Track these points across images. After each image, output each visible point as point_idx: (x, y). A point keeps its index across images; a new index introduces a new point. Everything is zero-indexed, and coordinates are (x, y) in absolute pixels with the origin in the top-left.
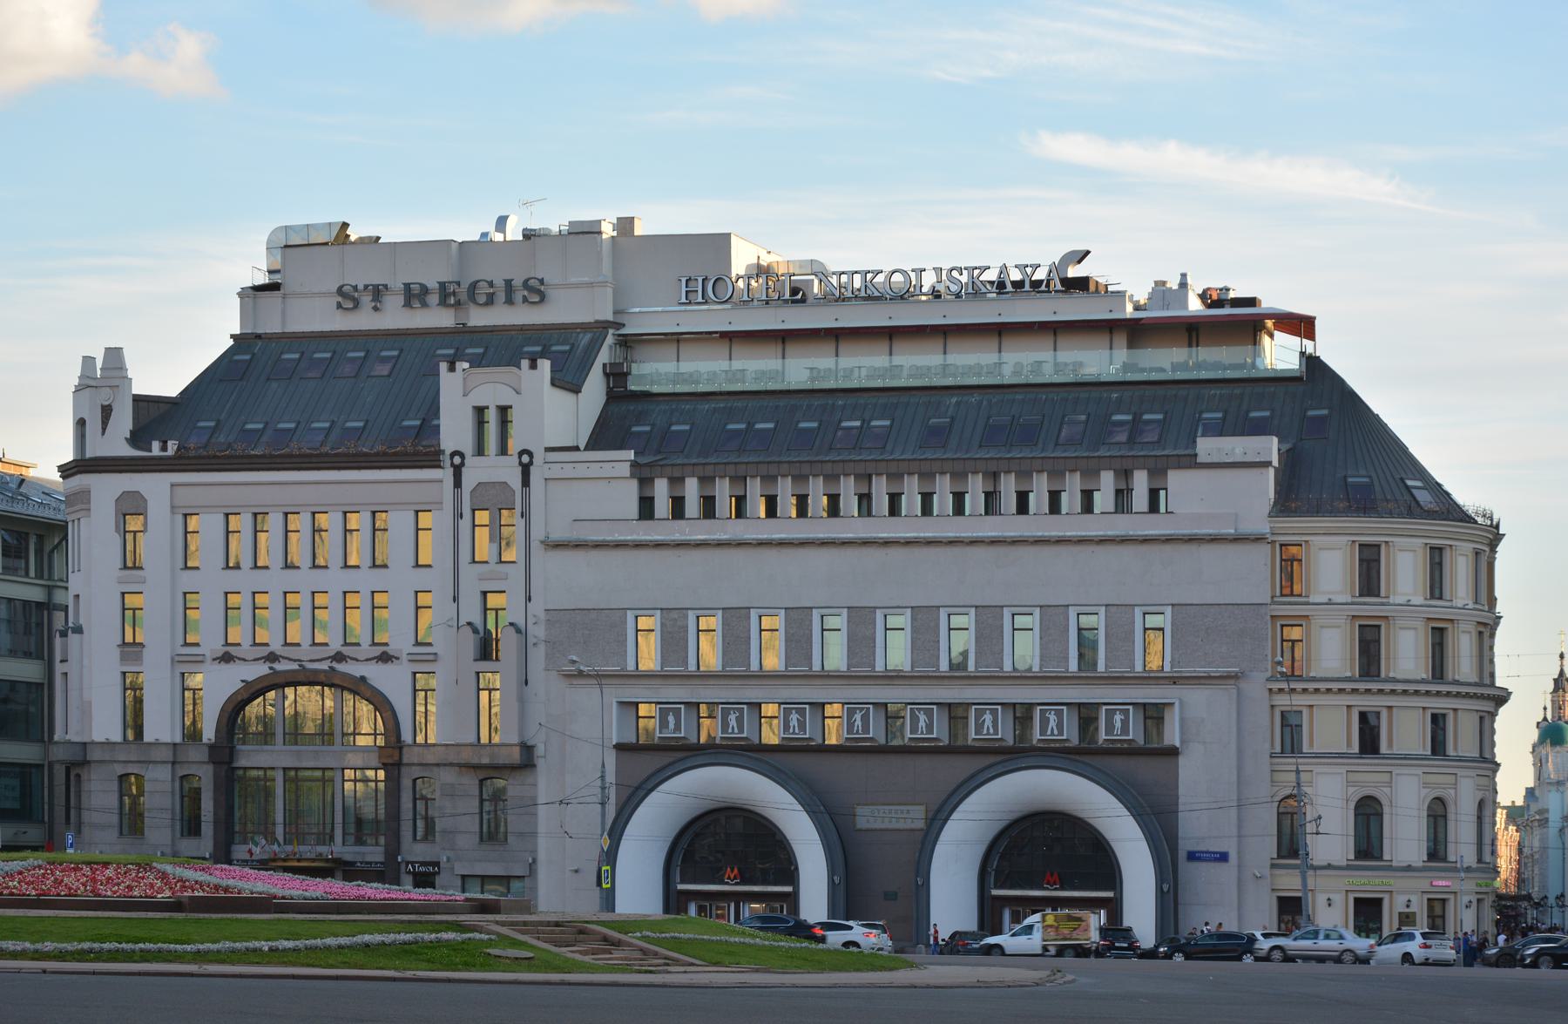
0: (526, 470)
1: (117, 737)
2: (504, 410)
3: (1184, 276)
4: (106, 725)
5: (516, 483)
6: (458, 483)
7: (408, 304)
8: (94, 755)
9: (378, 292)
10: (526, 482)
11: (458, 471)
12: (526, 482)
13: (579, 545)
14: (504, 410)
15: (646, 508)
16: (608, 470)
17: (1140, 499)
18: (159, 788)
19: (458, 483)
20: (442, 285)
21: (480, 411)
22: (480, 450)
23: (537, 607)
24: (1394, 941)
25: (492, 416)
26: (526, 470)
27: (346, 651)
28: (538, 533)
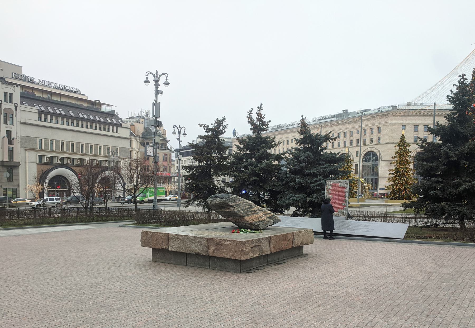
0: (16, 107)
2: (11, 94)
5: (14, 109)
14: (11, 94)
16: (33, 111)
22: (6, 101)
23: (19, 135)
26: (16, 107)
28: (19, 120)
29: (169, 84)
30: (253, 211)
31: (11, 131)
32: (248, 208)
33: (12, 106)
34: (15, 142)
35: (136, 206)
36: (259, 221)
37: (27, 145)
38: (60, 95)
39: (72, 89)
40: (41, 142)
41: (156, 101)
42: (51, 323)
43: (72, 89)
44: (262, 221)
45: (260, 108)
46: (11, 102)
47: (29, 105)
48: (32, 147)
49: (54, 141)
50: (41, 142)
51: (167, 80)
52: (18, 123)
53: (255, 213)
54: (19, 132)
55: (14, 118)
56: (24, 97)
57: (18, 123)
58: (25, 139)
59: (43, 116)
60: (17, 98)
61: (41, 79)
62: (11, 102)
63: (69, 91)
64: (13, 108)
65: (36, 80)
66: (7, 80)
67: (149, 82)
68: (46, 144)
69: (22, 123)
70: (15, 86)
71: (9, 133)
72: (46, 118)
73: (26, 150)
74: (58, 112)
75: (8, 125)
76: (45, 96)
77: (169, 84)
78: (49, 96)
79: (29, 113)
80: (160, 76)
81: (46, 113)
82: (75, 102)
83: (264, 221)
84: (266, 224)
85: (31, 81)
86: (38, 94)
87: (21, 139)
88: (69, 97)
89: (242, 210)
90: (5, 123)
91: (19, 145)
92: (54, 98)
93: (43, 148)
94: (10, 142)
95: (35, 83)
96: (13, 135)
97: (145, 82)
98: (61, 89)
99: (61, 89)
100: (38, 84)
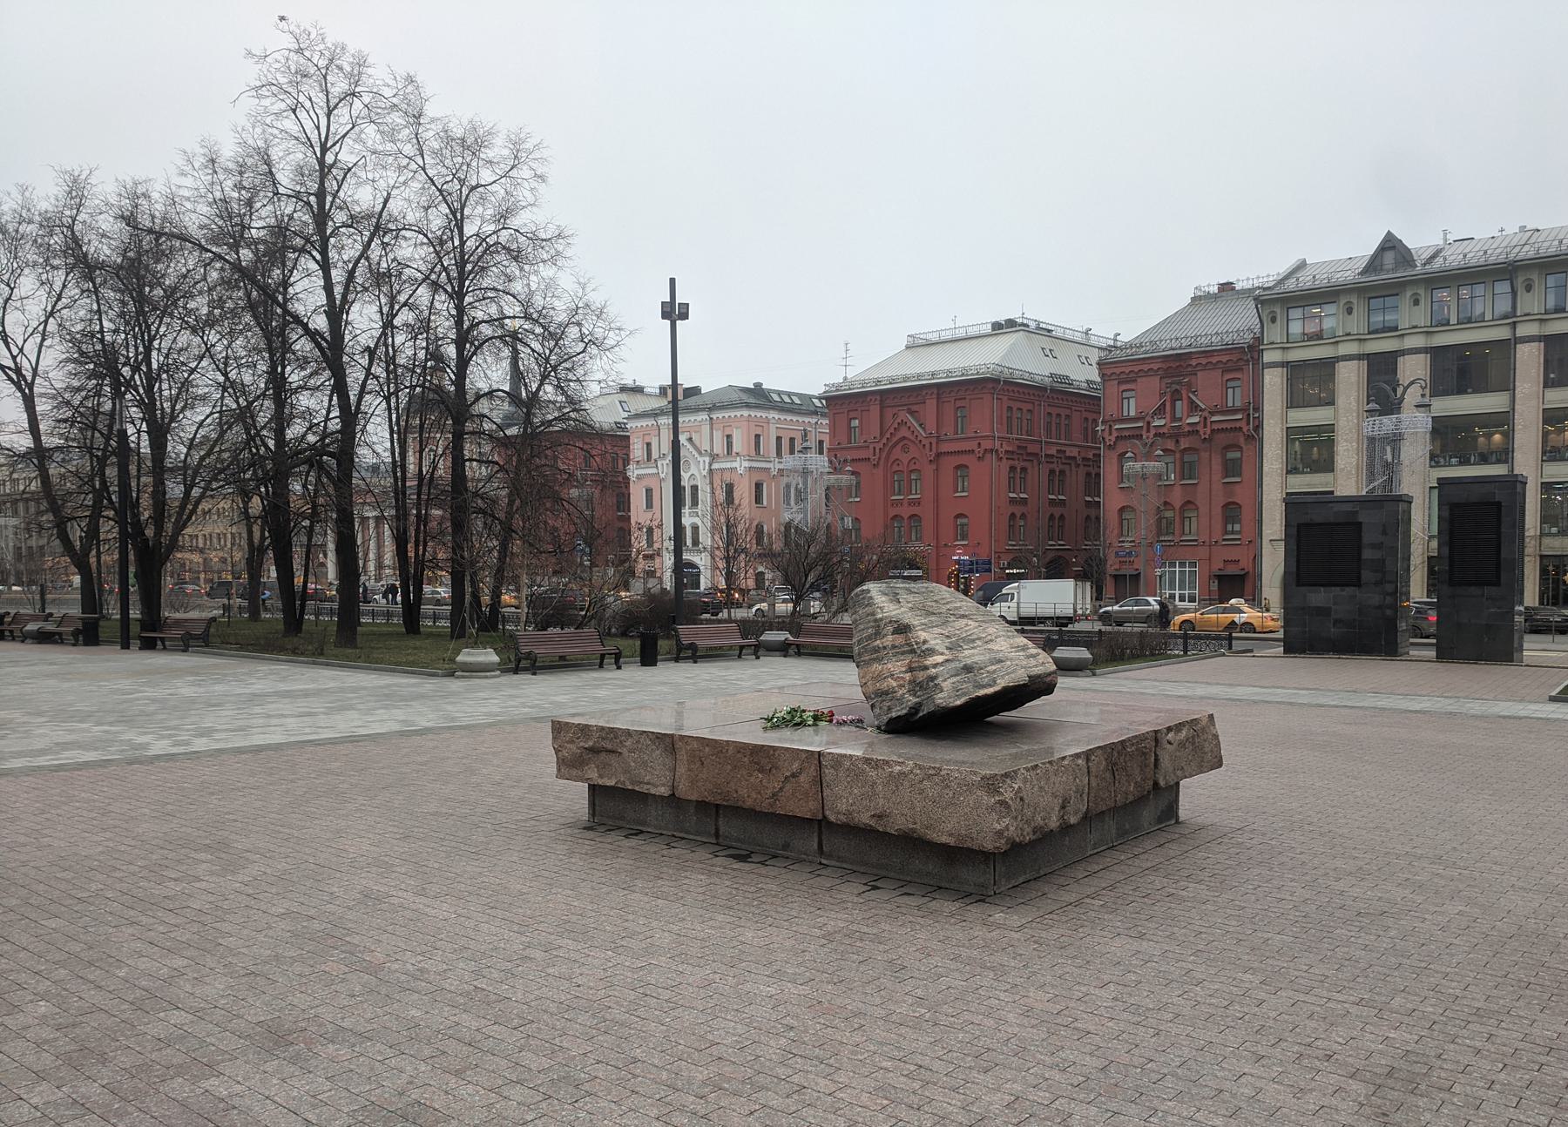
83: (886, 693)
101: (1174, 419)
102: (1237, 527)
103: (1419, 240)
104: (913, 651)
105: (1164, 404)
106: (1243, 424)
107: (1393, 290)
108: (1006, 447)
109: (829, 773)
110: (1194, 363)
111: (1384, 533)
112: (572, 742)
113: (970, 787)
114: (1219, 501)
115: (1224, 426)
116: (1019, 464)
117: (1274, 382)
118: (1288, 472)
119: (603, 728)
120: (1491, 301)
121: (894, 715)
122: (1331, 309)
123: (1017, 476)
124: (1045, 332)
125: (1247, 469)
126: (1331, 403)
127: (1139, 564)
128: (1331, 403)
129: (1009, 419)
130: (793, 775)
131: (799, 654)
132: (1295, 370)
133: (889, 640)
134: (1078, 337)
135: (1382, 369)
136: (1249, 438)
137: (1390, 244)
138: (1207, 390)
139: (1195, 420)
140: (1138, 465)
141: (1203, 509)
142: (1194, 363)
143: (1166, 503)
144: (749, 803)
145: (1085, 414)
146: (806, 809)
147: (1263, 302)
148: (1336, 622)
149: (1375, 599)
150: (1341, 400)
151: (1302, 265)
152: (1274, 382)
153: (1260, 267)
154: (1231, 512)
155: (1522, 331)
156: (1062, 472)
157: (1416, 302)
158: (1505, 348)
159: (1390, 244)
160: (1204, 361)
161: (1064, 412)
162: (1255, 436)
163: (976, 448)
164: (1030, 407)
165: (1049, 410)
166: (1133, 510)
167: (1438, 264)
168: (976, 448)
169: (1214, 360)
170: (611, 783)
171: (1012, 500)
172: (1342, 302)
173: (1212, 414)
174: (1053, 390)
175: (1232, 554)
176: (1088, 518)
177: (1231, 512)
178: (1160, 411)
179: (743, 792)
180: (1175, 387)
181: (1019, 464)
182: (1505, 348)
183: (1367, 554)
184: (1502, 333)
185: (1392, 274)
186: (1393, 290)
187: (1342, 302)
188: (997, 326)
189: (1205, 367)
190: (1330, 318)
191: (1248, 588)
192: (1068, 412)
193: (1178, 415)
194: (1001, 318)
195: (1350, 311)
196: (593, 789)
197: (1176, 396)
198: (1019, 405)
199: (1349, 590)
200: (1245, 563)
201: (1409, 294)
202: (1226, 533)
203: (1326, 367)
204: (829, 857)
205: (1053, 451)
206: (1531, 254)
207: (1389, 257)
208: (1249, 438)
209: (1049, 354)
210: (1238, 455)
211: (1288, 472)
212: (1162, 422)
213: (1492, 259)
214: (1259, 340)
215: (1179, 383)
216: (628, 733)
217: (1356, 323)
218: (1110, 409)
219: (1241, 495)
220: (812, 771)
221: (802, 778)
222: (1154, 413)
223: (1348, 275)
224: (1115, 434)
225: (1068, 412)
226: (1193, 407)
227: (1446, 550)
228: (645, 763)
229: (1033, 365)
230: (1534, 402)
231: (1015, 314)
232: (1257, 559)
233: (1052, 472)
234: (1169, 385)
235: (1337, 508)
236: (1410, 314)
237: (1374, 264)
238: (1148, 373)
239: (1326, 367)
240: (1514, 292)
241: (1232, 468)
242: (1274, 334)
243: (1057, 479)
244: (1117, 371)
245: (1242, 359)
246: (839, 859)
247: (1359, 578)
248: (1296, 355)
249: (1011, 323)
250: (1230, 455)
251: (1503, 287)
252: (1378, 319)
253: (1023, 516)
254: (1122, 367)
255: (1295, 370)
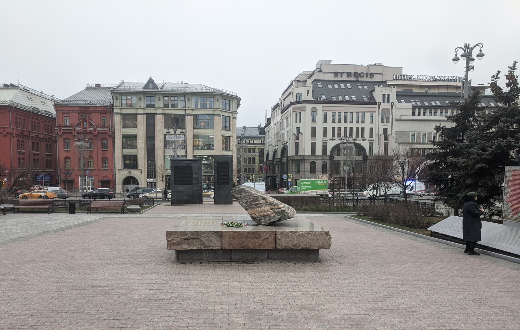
0: (392, 106)
1: (294, 154)
2: (389, 95)
3: (516, 63)
4: (308, 152)
5: (390, 108)
6: (379, 108)
7: (348, 76)
8: (305, 158)
9: (342, 73)
10: (392, 108)
11: (379, 106)
12: (392, 108)
13: (403, 120)
14: (389, 95)
15: (413, 114)
16: (408, 107)
17: (417, 113)
18: (319, 164)
19: (379, 108)
20: (354, 73)
21: (384, 95)
22: (384, 102)
23: (393, 131)
24: (431, 236)
25: (386, 96)
26: (392, 106)
27: (357, 138)
28: (394, 118)
29: (483, 55)
30: (256, 204)
31: (387, 128)
32: (252, 201)
33: (389, 106)
34: (390, 138)
35: (406, 199)
36: (261, 216)
37: (401, 140)
38: (438, 87)
39: (451, 78)
40: (413, 136)
41: (466, 78)
42: (176, 283)
43: (451, 78)
44: (264, 216)
45: (513, 68)
46: (388, 102)
47: (406, 103)
48: (405, 141)
49: (427, 133)
50: (413, 136)
51: (481, 51)
52: (394, 120)
53: (259, 207)
54: (394, 128)
55: (391, 116)
56: (400, 96)
57: (394, 120)
58: (400, 134)
59: (417, 110)
60: (393, 98)
61: (419, 75)
62: (388, 102)
63: (448, 81)
64: (390, 107)
65: (415, 77)
66: (388, 83)
67: (458, 59)
68: (419, 137)
69: (396, 120)
70: (392, 87)
71: (385, 130)
72: (436, 112)
73: (399, 144)
74: (434, 104)
75: (385, 123)
76: (423, 91)
77: (483, 55)
78: (427, 89)
79: (403, 110)
80: (472, 49)
81: (419, 108)
82: (444, 91)
83: (267, 216)
84: (269, 220)
85: (410, 79)
86: (415, 90)
87: (396, 134)
88: (447, 87)
89: (246, 203)
90: (383, 121)
91: (394, 140)
92: (432, 91)
93: (416, 141)
94: (386, 138)
95: (414, 80)
96: (389, 132)
97: (454, 60)
98: (439, 81)
99: (439, 81)
100: (417, 80)
101: (84, 128)
102: (107, 165)
103: (158, 81)
104: (270, 204)
105: (80, 122)
106: (108, 132)
107: (154, 95)
108: (15, 132)
109: (279, 236)
110: (90, 110)
111: (198, 170)
112: (178, 237)
113: (322, 235)
114: (100, 157)
115: (102, 132)
116: (21, 139)
117: (117, 119)
118: (123, 148)
119: (192, 232)
120: (180, 102)
121: (272, 221)
122: (134, 98)
123: (20, 144)
124: (25, 90)
125: (110, 146)
126: (136, 127)
127: (72, 177)
128: (136, 127)
129: (16, 122)
130: (267, 238)
131: (18, 212)
132: (124, 116)
133: (262, 202)
134: (40, 94)
135: (150, 119)
136: (110, 136)
137: (151, 81)
138: (96, 119)
139: (92, 129)
140: (80, 143)
141: (95, 159)
142: (90, 110)
143: (90, 156)
144: (251, 247)
145: (45, 123)
146: (270, 246)
147: (113, 93)
148: (186, 195)
149: (197, 189)
150: (139, 127)
151: (123, 83)
152: (117, 119)
153: (111, 81)
154: (105, 160)
155: (188, 112)
156: (37, 143)
157: (160, 100)
158: (184, 116)
159: (151, 81)
160: (94, 110)
161: (37, 121)
162: (112, 136)
163: (3, 132)
164: (24, 118)
165: (32, 120)
166: (70, 158)
167: (165, 89)
168: (3, 132)
169: (98, 110)
170: (195, 248)
171: (19, 153)
172: (138, 96)
173: (97, 127)
174: (33, 113)
175: (106, 174)
176: (47, 160)
177: (105, 160)
178: (79, 125)
179: (249, 245)
180: (84, 117)
181: (36, 142)
182: (184, 116)
183: (194, 176)
184: (182, 112)
185: (151, 91)
186: (154, 95)
187: (138, 96)
188: (6, 86)
189: (94, 112)
190: (134, 100)
191: (111, 185)
192: (38, 121)
193: (85, 127)
194: (8, 83)
195: (140, 100)
196: (178, 252)
197: (84, 120)
198: (20, 117)
199: (189, 186)
200: (110, 177)
201: (158, 97)
202: (103, 167)
203: (134, 116)
204: (271, 259)
205: (34, 135)
206: (189, 91)
207: (151, 85)
208: (110, 136)
209: (30, 99)
210: (106, 142)
211: (123, 148)
212: (80, 129)
213: (179, 90)
214: (112, 105)
215: (85, 116)
216: (204, 232)
217: (143, 104)
218: (59, 122)
219: (108, 155)
220: (273, 236)
221: (270, 238)
222: (77, 125)
223: (140, 88)
224: (62, 131)
225: (38, 121)
226: (91, 125)
227: (216, 175)
228: (210, 241)
229: (23, 102)
230: (191, 133)
231: (15, 83)
232: (114, 175)
233: (33, 143)
234: (82, 116)
235: (186, 162)
236: (159, 104)
237: (146, 86)
238: (74, 111)
239: (134, 116)
240: (185, 101)
241: (104, 146)
242: (117, 103)
243: (35, 146)
244: (62, 109)
245: (107, 110)
246: (274, 259)
247: (192, 182)
248: (125, 111)
249: (12, 86)
250: (105, 141)
251: (182, 99)
252: (148, 103)
253: (23, 159)
254: (63, 108)
255: (124, 116)
